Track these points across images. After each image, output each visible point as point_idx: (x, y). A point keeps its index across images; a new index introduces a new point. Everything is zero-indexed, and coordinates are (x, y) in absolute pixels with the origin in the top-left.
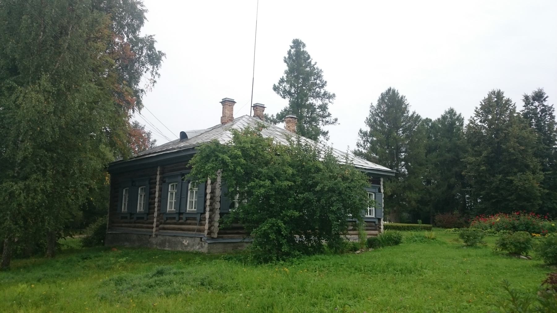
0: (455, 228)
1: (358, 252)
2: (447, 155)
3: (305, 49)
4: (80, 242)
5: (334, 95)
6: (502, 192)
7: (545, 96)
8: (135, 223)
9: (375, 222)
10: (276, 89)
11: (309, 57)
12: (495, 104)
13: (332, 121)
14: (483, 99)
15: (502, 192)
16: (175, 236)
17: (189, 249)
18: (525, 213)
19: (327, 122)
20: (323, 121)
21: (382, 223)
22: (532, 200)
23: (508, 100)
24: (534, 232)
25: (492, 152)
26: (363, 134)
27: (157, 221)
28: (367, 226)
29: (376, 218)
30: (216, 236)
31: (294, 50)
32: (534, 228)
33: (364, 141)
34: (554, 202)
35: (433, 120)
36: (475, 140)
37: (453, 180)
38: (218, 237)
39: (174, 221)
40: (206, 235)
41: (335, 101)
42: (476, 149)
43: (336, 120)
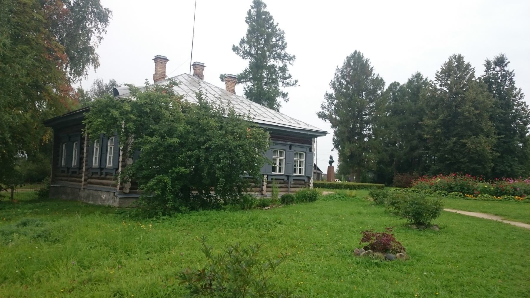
0: (397, 187)
1: (266, 208)
2: (411, 118)
3: (265, 10)
4: (36, 194)
5: (294, 56)
6: (456, 154)
7: (507, 61)
8: (71, 177)
9: (304, 180)
10: (235, 49)
11: (271, 18)
12: (456, 69)
13: (292, 82)
14: (444, 63)
15: (456, 154)
16: (96, 190)
17: (107, 203)
18: (461, 175)
19: (288, 83)
20: (283, 82)
21: (312, 181)
22: (483, 163)
23: (468, 65)
24: (467, 193)
25: (450, 115)
27: (85, 175)
28: (294, 184)
29: (305, 176)
30: (128, 191)
31: (255, 10)
32: (468, 189)
33: (329, 103)
34: (507, 165)
35: (401, 84)
36: (432, 104)
37: (415, 143)
38: (130, 193)
39: (98, 176)
40: (118, 190)
41: (295, 62)
42: (433, 112)
43: (296, 82)
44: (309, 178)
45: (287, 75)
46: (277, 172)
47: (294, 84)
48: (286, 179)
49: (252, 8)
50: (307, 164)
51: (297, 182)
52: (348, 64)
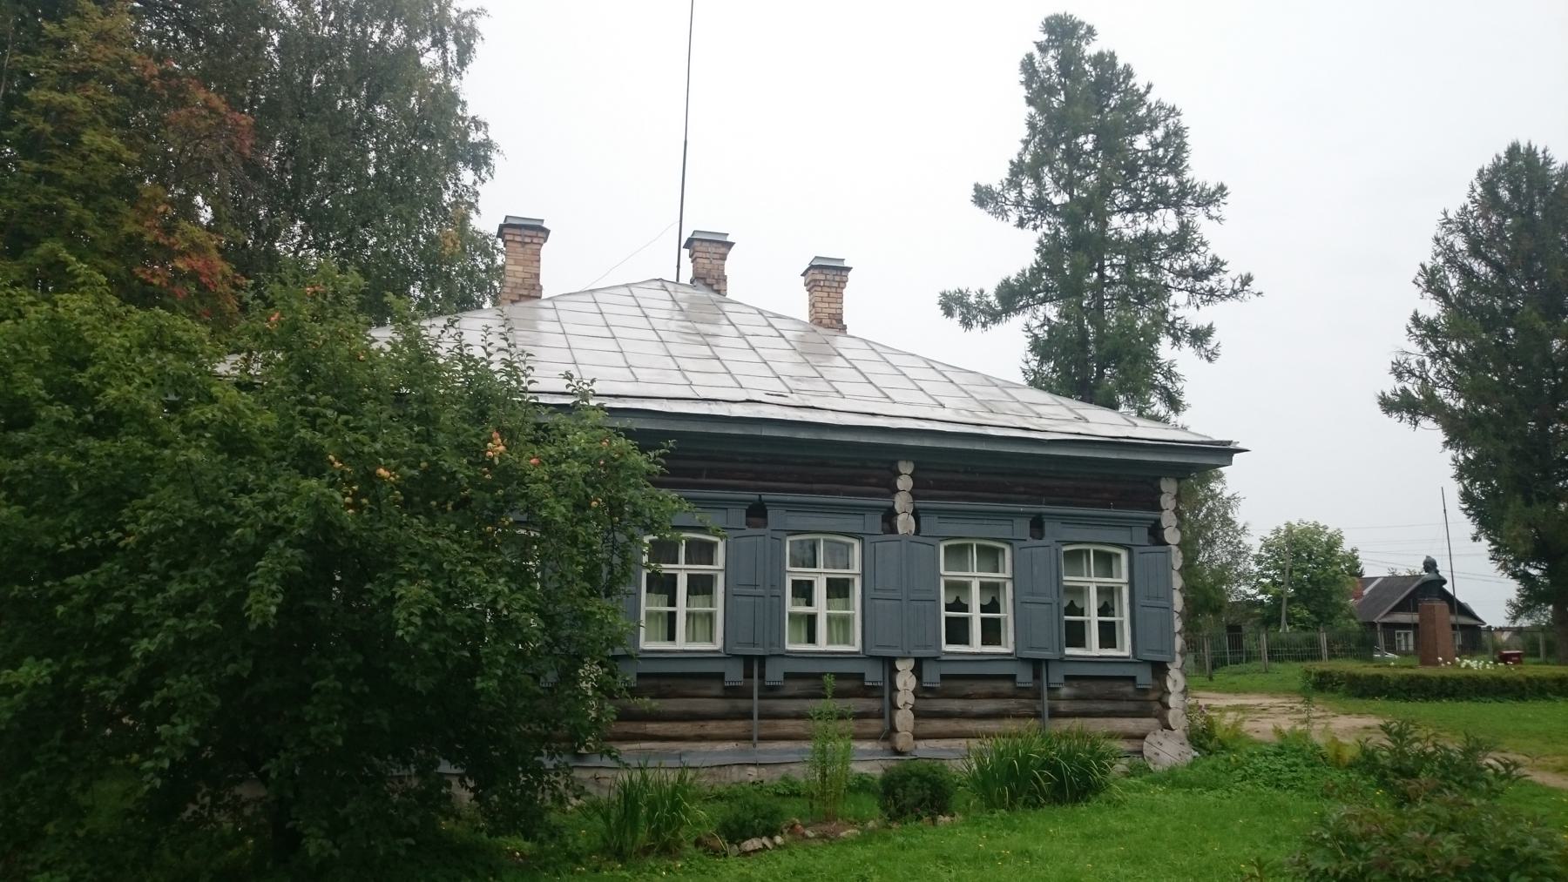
5: (1222, 188)
10: (983, 197)
13: (1228, 284)
19: (1212, 292)
26: (1426, 330)
28: (1077, 698)
29: (1136, 660)
43: (1247, 280)
44: (1160, 669)
45: (1201, 260)
46: (1093, 648)
47: (1235, 292)
48: (1025, 677)
49: (1043, 48)
50: (1139, 600)
51: (1095, 688)
52: (1489, 198)
